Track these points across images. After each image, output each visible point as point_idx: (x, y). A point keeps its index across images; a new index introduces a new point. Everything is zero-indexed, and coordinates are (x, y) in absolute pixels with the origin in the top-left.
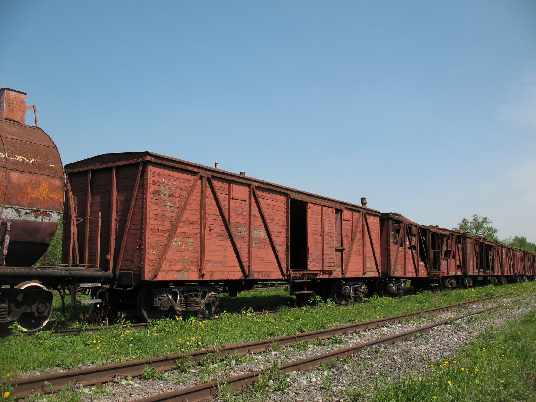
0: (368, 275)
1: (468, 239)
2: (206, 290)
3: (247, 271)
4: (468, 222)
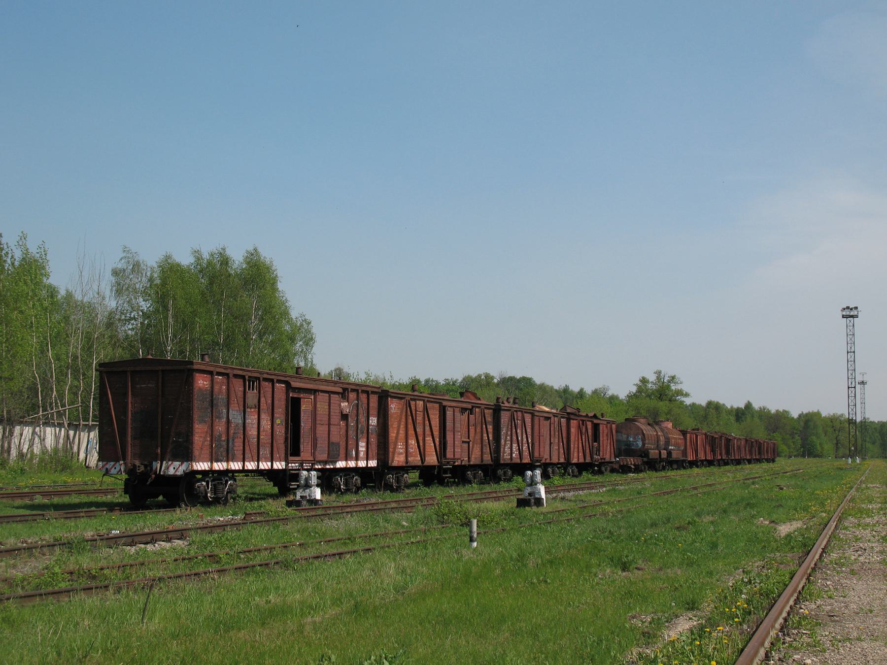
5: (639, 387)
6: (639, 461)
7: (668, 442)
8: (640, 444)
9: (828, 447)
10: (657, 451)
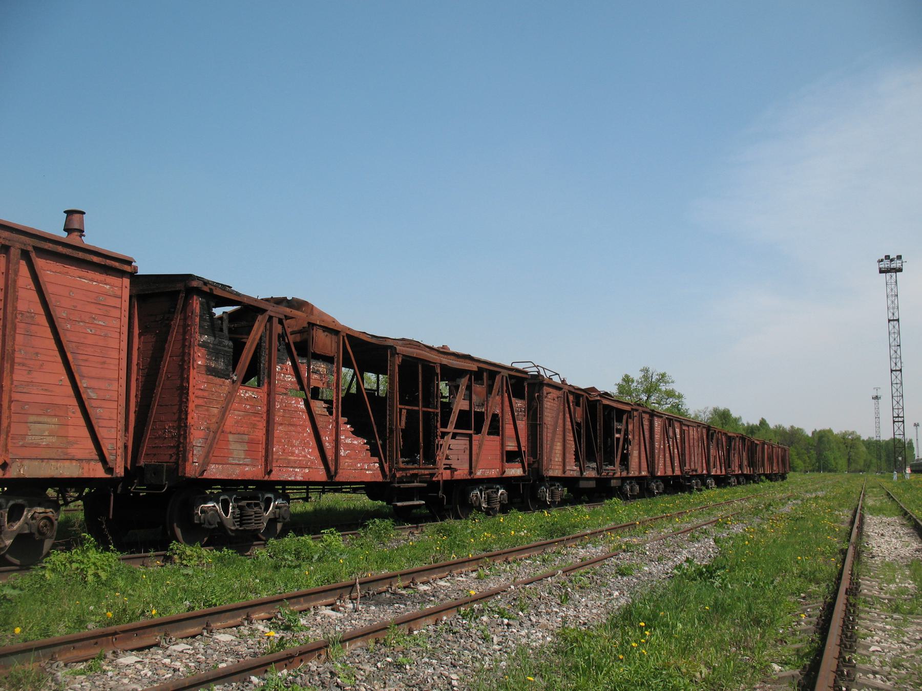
0: (569, 474)
1: (546, 389)
2: (20, 501)
3: (332, 469)
4: (633, 381)
5: (620, 387)
9: (843, 462)
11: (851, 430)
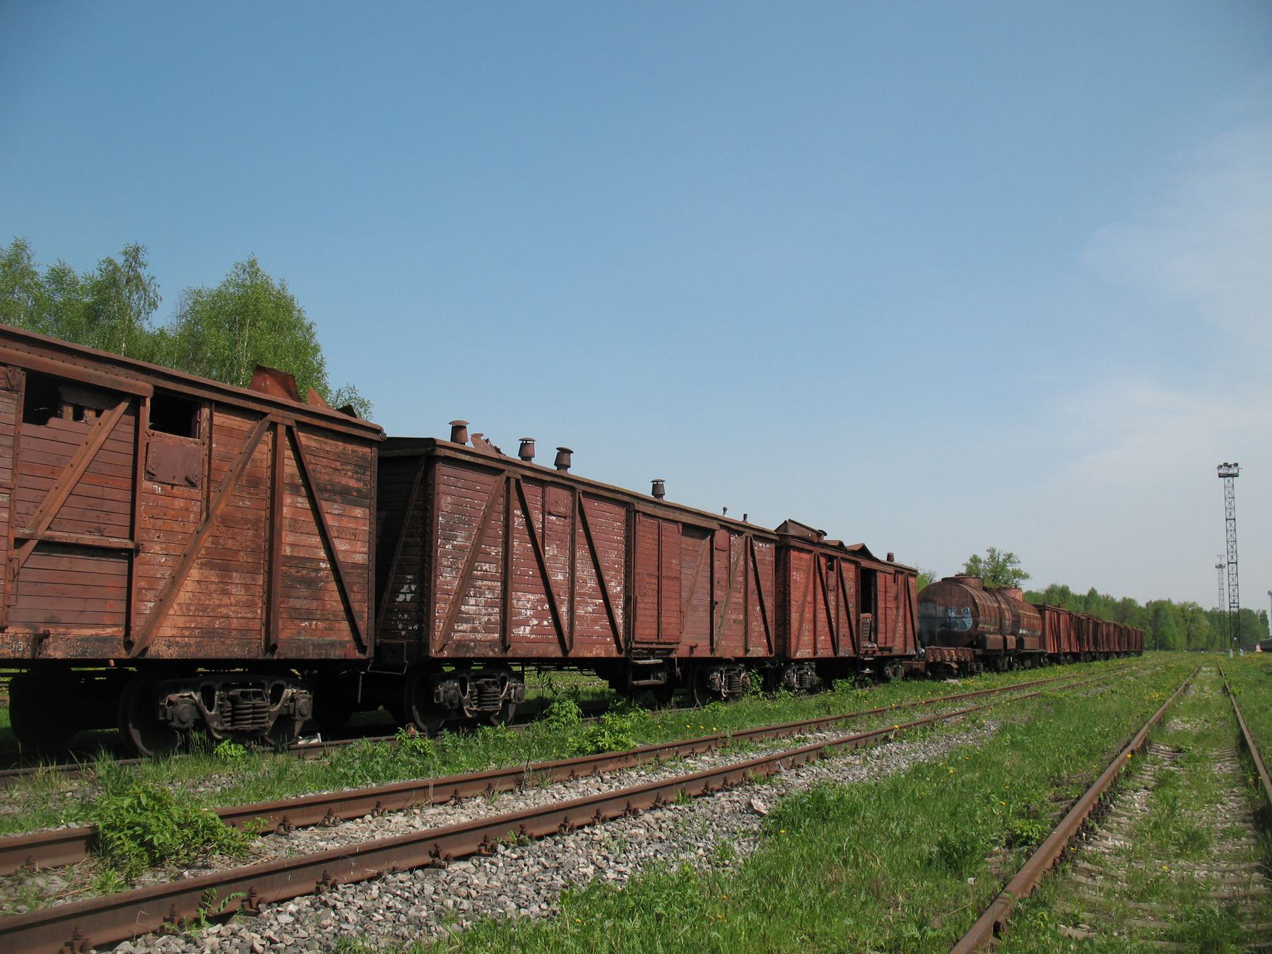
0: (821, 654)
2: (278, 682)
5: (969, 567)
6: (966, 654)
7: (1017, 623)
8: (969, 622)
9: (1181, 639)
10: (1000, 637)
11: (1191, 601)
